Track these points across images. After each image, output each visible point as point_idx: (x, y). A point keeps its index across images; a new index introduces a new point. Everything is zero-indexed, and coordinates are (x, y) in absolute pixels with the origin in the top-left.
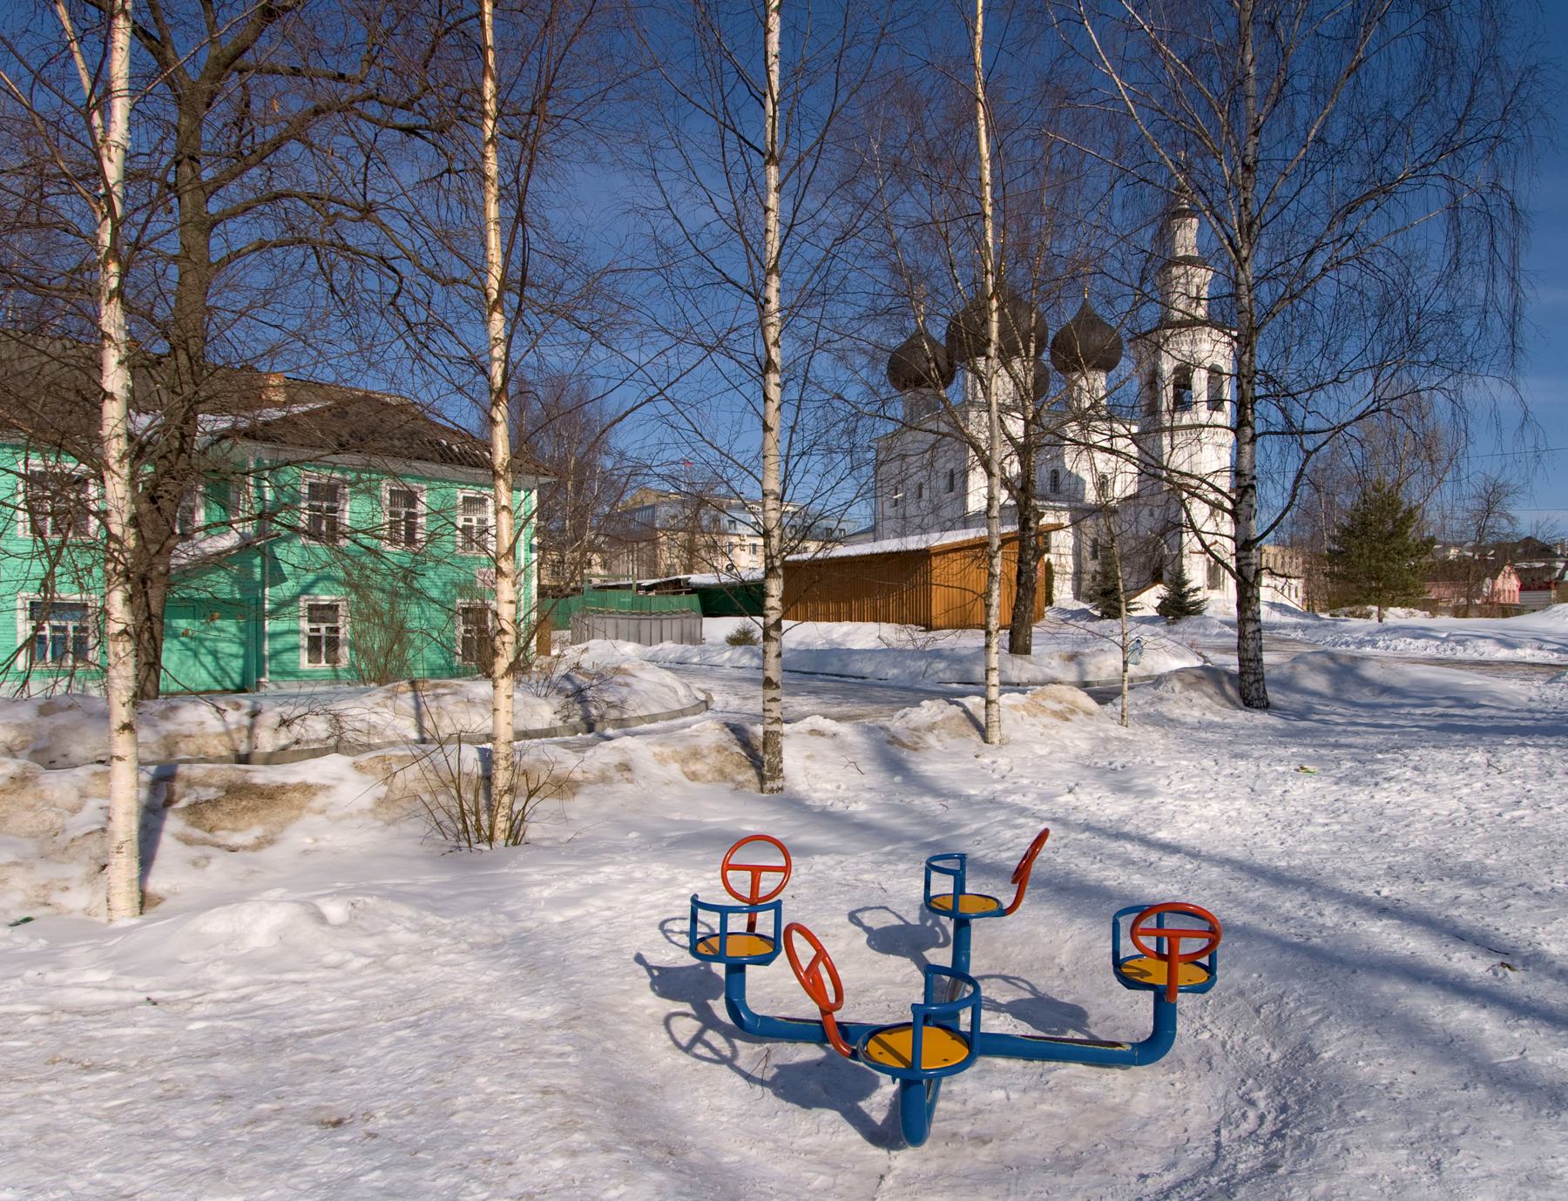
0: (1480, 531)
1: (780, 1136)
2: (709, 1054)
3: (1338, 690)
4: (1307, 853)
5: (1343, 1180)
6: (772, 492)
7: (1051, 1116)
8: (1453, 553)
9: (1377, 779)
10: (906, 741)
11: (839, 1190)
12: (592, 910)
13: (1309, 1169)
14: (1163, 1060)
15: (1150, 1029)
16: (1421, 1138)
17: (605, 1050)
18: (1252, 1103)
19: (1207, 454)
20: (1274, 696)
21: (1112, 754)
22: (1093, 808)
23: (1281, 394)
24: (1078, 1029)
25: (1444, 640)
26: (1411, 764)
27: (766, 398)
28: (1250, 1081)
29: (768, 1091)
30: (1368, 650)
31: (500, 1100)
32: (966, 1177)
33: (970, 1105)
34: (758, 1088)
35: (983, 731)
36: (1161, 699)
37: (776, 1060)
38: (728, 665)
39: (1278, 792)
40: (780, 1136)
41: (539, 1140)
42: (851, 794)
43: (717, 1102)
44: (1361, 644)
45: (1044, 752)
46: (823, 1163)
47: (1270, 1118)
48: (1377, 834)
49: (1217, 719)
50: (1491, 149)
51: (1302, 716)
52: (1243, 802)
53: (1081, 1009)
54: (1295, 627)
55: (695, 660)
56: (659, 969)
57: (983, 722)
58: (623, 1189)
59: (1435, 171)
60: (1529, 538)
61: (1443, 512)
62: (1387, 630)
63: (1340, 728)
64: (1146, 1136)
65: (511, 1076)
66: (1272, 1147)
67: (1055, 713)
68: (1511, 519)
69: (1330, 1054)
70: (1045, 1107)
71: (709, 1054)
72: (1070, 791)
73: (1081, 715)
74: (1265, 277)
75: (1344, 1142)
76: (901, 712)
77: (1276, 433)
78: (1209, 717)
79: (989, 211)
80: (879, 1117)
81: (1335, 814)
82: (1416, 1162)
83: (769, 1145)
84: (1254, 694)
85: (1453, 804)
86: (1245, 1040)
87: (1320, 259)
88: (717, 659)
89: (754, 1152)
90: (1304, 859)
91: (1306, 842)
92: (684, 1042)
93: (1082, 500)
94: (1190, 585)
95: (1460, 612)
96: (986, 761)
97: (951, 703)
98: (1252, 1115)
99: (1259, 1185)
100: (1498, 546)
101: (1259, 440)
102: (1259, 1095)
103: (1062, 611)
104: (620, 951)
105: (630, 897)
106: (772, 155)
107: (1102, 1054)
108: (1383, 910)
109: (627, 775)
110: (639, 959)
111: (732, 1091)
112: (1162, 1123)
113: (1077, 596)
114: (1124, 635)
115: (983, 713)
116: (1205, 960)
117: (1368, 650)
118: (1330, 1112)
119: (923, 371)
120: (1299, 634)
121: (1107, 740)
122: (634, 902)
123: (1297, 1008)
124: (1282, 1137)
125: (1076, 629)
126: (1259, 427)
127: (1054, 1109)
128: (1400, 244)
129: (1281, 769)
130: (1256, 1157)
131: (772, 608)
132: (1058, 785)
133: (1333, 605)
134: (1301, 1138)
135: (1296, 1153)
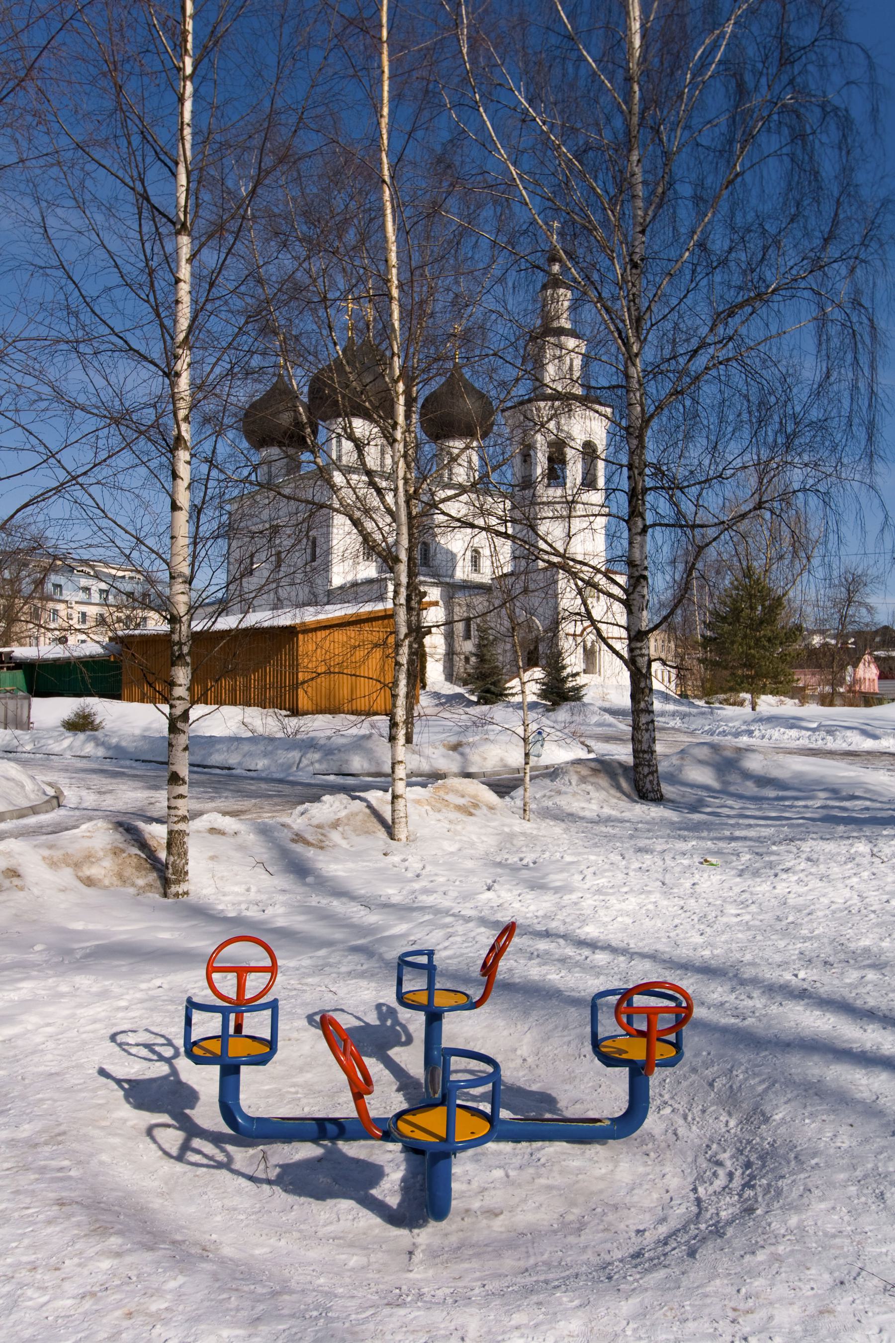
0: (843, 619)
1: (302, 1227)
2: (205, 1161)
3: (726, 783)
4: (726, 942)
5: (810, 1213)
6: (181, 575)
7: (550, 1188)
8: (817, 640)
9: (775, 870)
10: (310, 838)
11: (376, 1266)
12: (30, 1027)
13: (781, 1208)
14: (634, 1135)
15: (625, 1106)
16: (866, 1177)
17: (101, 1163)
18: (719, 1164)
19: (590, 541)
20: (667, 790)
21: (519, 850)
22: (517, 905)
23: (673, 488)
24: (550, 1112)
25: (814, 730)
26: (804, 856)
27: (175, 476)
28: (714, 1146)
29: (276, 1188)
30: (745, 740)
31: (16, 1215)
32: (486, 1245)
33: (475, 1185)
34: (265, 1187)
35: (390, 830)
36: (559, 793)
37: (274, 1160)
38: (68, 755)
39: (688, 885)
40: (302, 1227)
41: (77, 1246)
42: (264, 897)
43: (228, 1203)
44: (737, 734)
45: (453, 849)
46: (351, 1245)
47: (738, 1173)
48: (784, 923)
49: (614, 813)
50: (852, 270)
51: (694, 808)
52: (658, 895)
53: (549, 1096)
54: (674, 714)
55: (28, 748)
56: (128, 1081)
57: (389, 819)
58: (181, 1279)
59: (803, 285)
60: (886, 628)
61: (808, 597)
62: (761, 720)
63: (732, 821)
64: (635, 1199)
65: (17, 1192)
66: (746, 1196)
67: (459, 808)
68: (870, 609)
69: (780, 1115)
70: (543, 1181)
71: (205, 1161)
72: (489, 889)
73: (485, 810)
74: (654, 372)
75: (805, 1185)
76: (300, 808)
77: (667, 525)
78: (607, 811)
79: (395, 293)
80: (393, 1201)
81: (744, 904)
82: (865, 1195)
83: (296, 1235)
84: (648, 786)
85: (847, 893)
86: (704, 1111)
87: (702, 360)
88: (56, 747)
89: (283, 1242)
90: (726, 947)
91: (723, 932)
92: (174, 1151)
93: (452, 576)
94: (568, 670)
95: (826, 700)
96: (396, 859)
97: (354, 798)
98: (721, 1172)
99: (744, 1224)
100: (858, 634)
101: (650, 530)
102: (725, 1157)
103: (437, 695)
104: (79, 1066)
105: (67, 1012)
106: (184, 225)
107: (584, 1132)
108: (801, 995)
109: (16, 881)
110: (102, 1072)
111: (239, 1191)
112: (645, 1187)
113: (450, 676)
114: (526, 725)
115: (389, 807)
116: (672, 1037)
117: (745, 740)
118: (789, 1163)
119: (281, 429)
120: (676, 723)
121: (511, 836)
122: (73, 1016)
123: (746, 1079)
124: (753, 1187)
125: (461, 715)
126: (650, 518)
127: (550, 1182)
128: (774, 350)
129: (686, 862)
130: (733, 1205)
131: (180, 698)
132: (477, 882)
133: (708, 691)
134: (769, 1185)
135: (767, 1197)
